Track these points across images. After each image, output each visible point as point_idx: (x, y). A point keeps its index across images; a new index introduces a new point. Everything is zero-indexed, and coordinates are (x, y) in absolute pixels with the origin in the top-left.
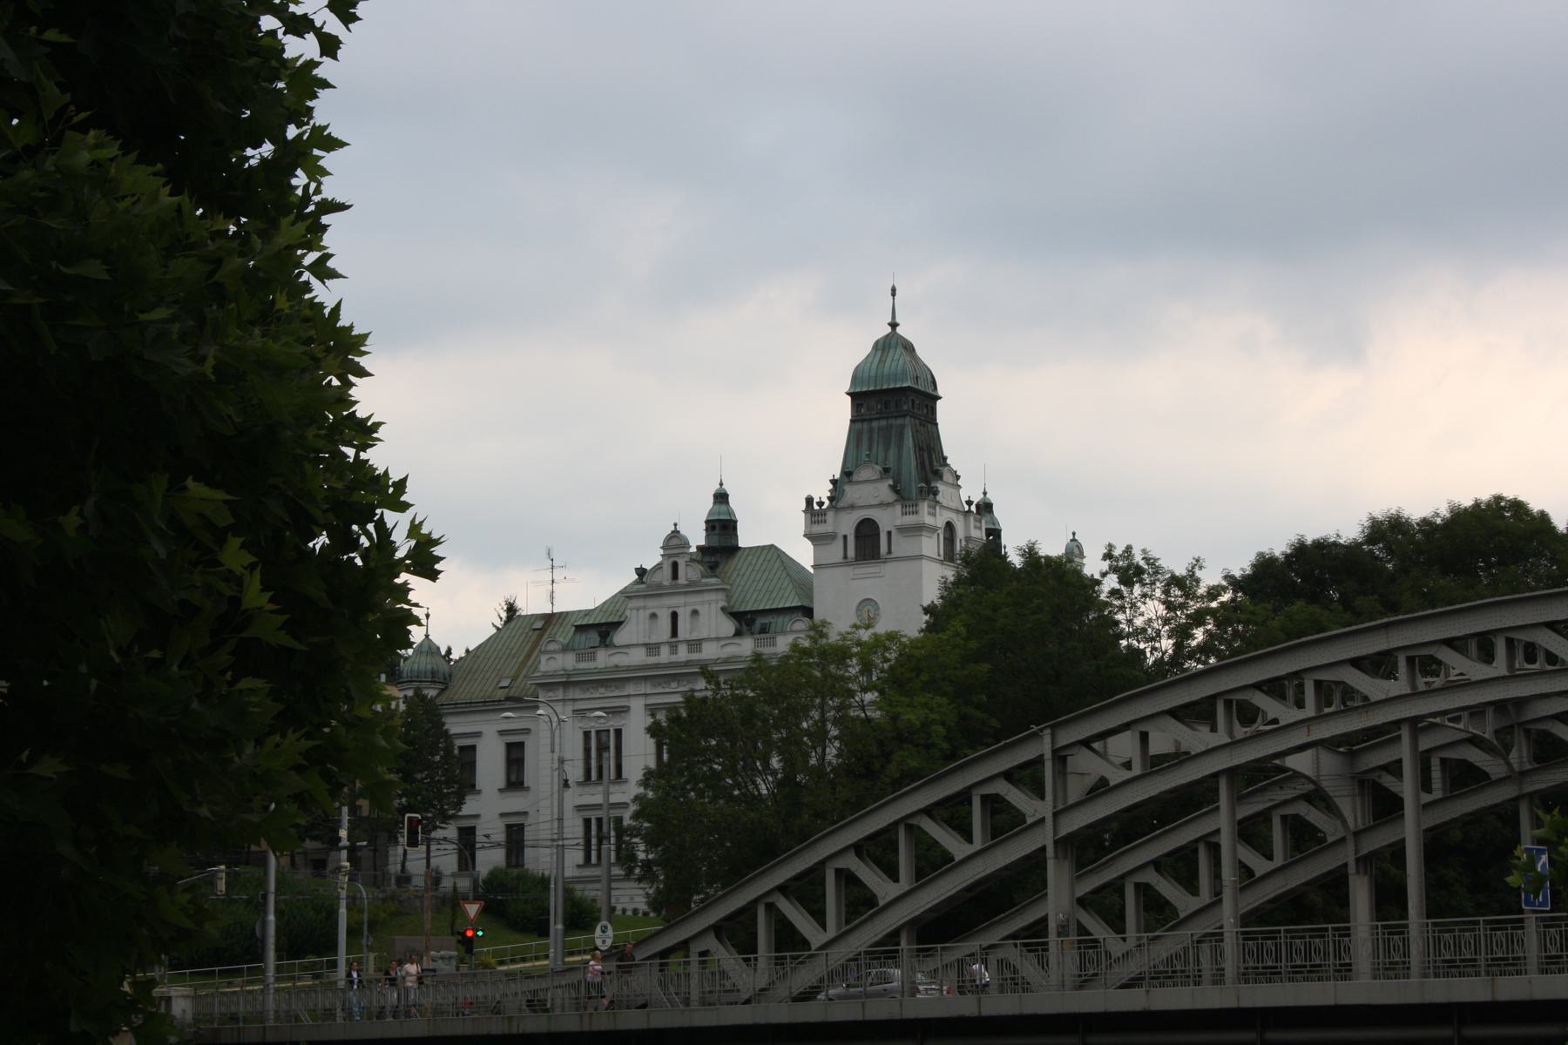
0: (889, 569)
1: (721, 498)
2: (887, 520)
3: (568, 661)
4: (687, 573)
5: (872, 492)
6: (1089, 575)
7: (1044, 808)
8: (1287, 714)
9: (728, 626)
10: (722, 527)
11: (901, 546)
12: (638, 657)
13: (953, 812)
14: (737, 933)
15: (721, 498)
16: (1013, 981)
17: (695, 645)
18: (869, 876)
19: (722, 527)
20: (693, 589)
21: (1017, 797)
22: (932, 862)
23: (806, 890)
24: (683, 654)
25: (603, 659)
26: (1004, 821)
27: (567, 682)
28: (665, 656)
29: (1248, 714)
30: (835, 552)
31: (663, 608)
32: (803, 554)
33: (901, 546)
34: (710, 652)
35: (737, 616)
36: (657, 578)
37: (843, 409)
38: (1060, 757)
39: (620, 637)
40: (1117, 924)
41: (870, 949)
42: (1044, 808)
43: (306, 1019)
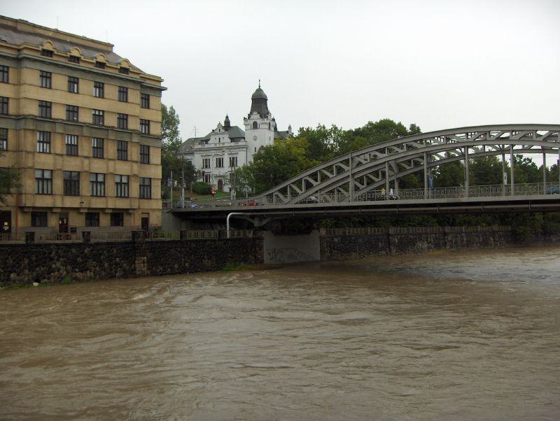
0: (259, 130)
1: (227, 117)
2: (259, 121)
3: (200, 146)
4: (222, 131)
5: (256, 116)
6: (397, 123)
7: (350, 168)
8: (400, 151)
9: (229, 141)
10: (227, 122)
11: (262, 126)
12: (213, 146)
13: (329, 169)
14: (284, 191)
15: (227, 117)
16: (280, 201)
17: (223, 144)
18: (311, 181)
19: (227, 122)
20: (223, 133)
21: (343, 166)
22: (324, 178)
23: (299, 183)
24: (221, 145)
25: (206, 146)
26: (340, 170)
27: (200, 150)
28: (218, 145)
29: (390, 150)
30: (249, 127)
31: (217, 137)
32: (243, 128)
33: (262, 126)
34: (226, 145)
35: (230, 138)
36: (216, 132)
37: (250, 102)
38: (352, 159)
39: (209, 142)
40: (347, 190)
41: (544, 173)
42: (350, 168)
43: (77, 221)
